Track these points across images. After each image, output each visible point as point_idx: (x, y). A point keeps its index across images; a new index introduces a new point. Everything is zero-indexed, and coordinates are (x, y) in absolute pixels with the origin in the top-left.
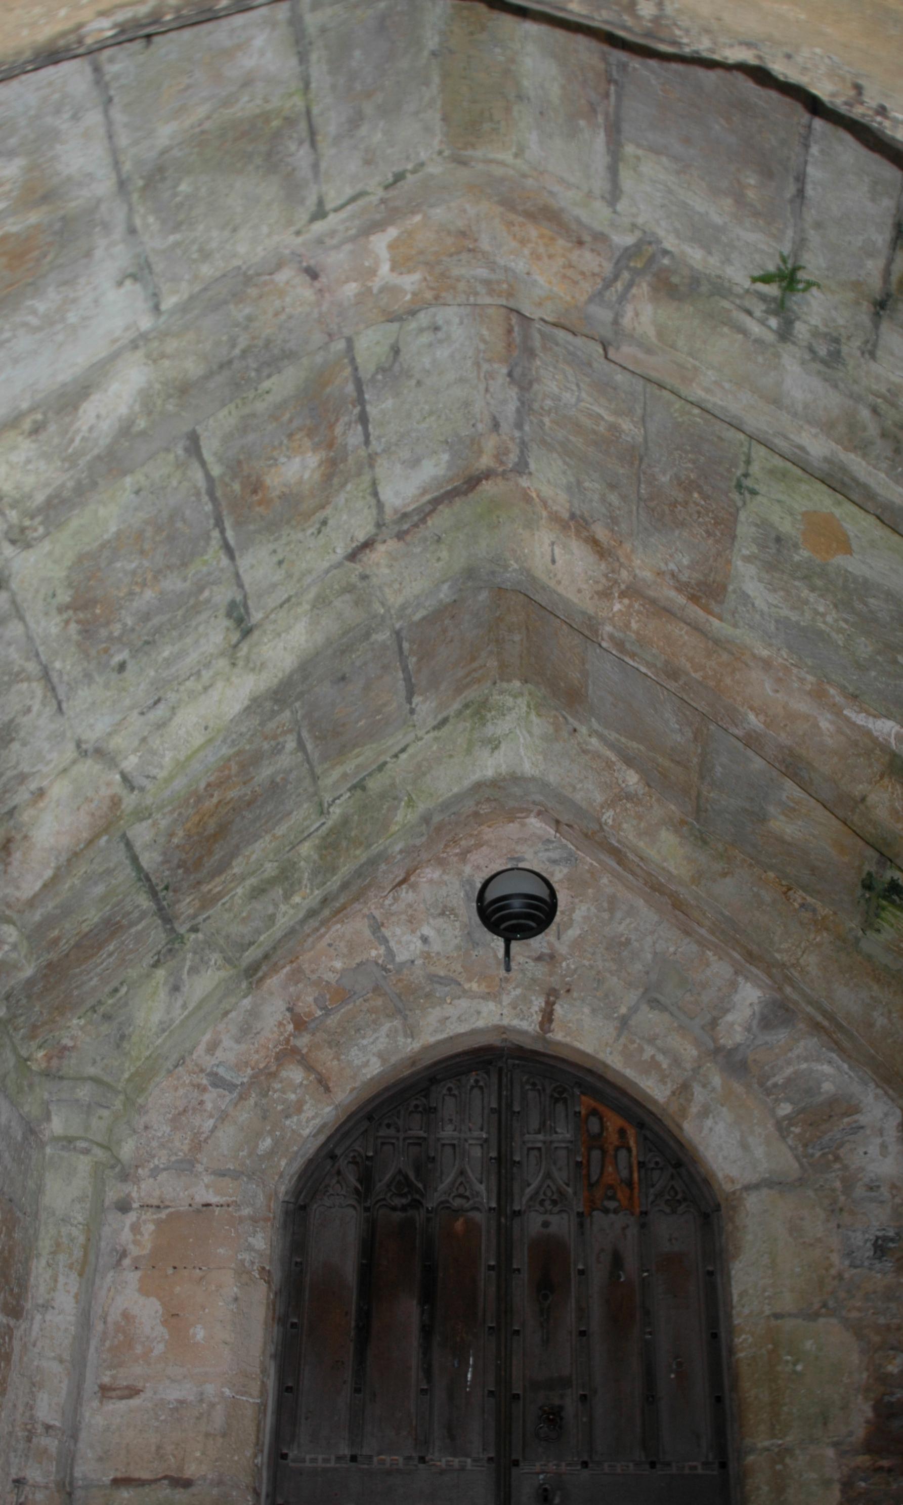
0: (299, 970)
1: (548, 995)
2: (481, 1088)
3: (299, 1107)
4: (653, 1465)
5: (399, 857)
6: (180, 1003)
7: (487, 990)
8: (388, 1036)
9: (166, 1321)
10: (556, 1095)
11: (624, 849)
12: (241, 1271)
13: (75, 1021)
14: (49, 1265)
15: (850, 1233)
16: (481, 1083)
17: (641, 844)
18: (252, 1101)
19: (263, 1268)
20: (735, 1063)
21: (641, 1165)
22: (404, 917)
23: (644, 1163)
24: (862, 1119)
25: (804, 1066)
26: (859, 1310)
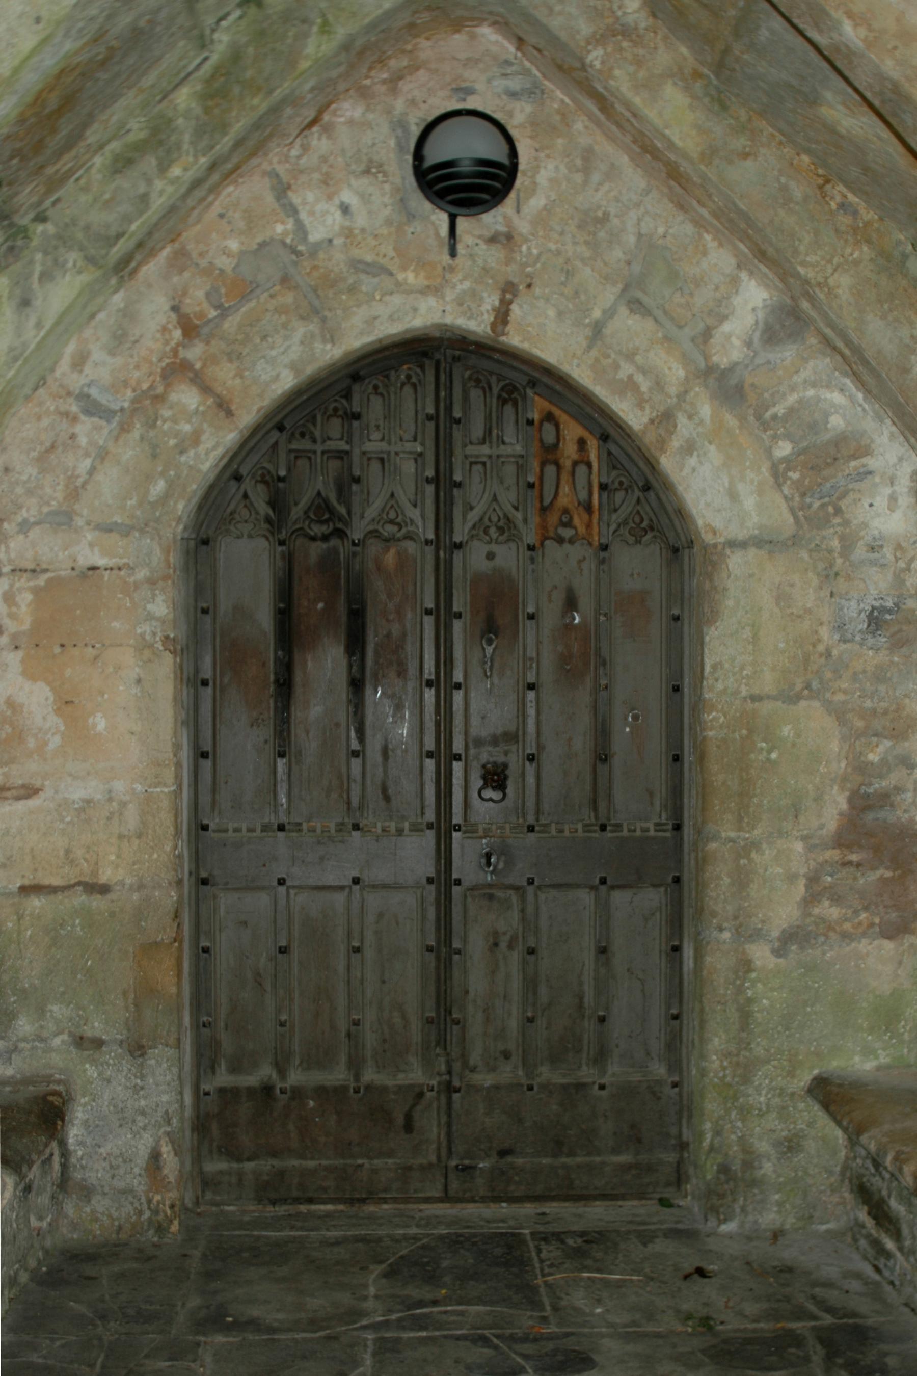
0: (182, 253)
1: (504, 291)
2: (414, 386)
3: (195, 439)
4: (603, 828)
5: (309, 96)
6: (32, 321)
7: (426, 283)
8: (302, 343)
9: (59, 709)
10: (505, 395)
11: (612, 99)
12: (143, 646)
15: (843, 602)
16: (414, 380)
17: (637, 101)
18: (136, 434)
19: (167, 637)
20: (729, 388)
21: (603, 487)
22: (316, 176)
23: (606, 485)
24: (872, 463)
25: (811, 393)
26: (845, 692)
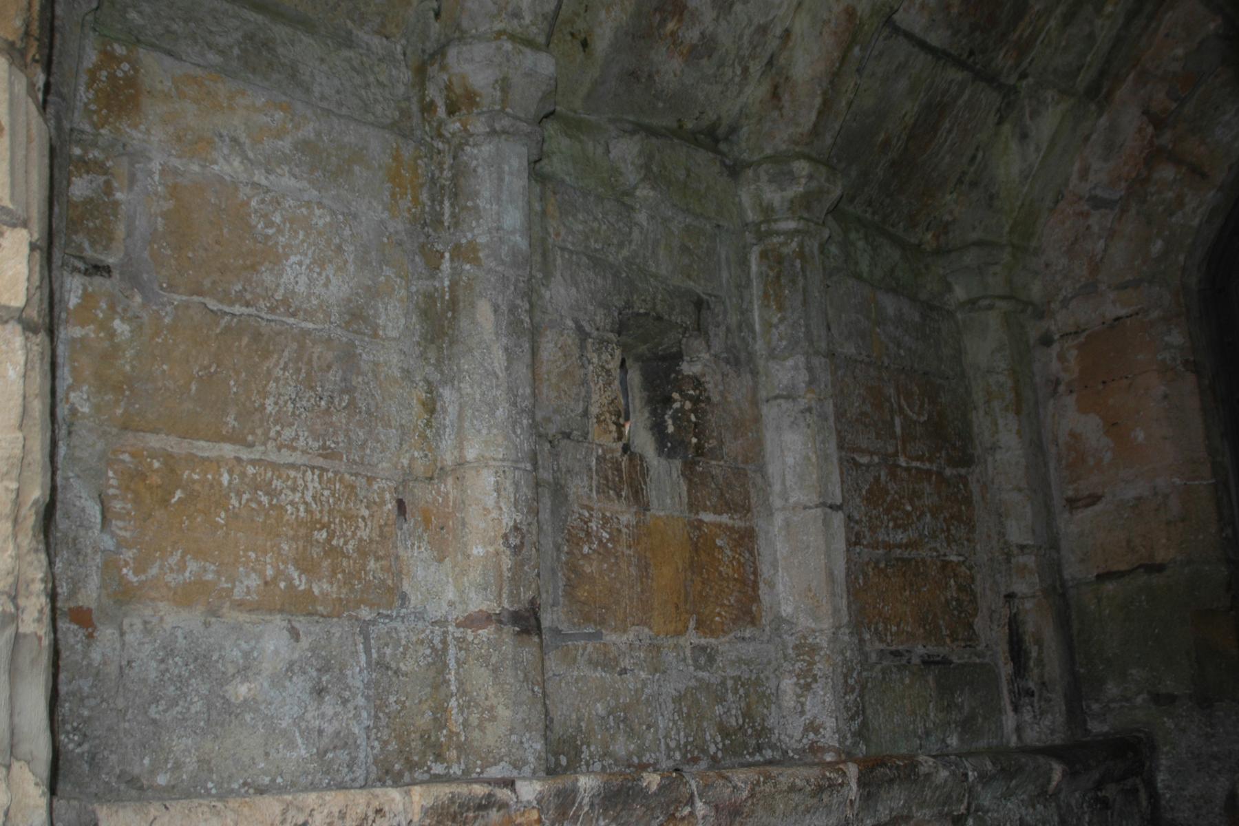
6: (1032, 148)
13: (948, 197)
14: (986, 413)
